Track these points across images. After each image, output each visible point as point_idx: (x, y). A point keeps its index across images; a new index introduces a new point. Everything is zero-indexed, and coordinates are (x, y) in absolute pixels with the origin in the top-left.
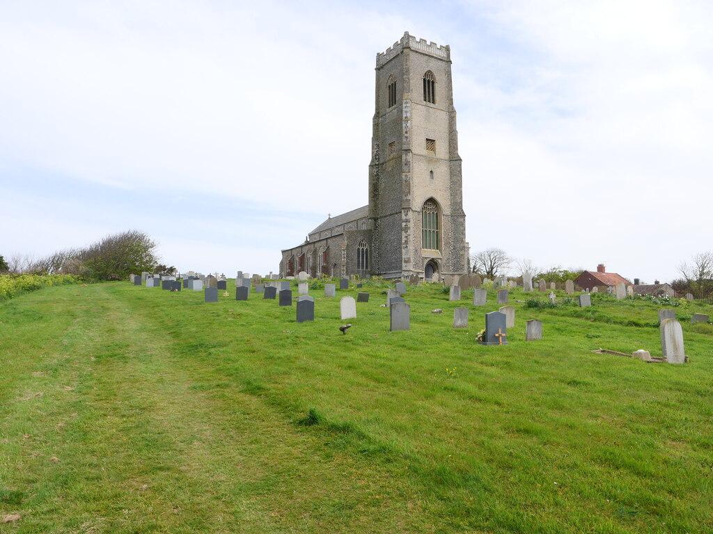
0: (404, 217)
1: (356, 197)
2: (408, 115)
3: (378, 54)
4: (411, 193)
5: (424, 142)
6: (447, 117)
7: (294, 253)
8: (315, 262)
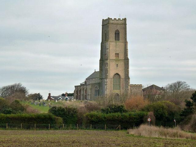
0: (106, 81)
1: (98, 69)
2: (108, 47)
3: (103, 19)
4: (108, 72)
5: (114, 55)
6: (124, 45)
7: (79, 87)
8: (83, 93)
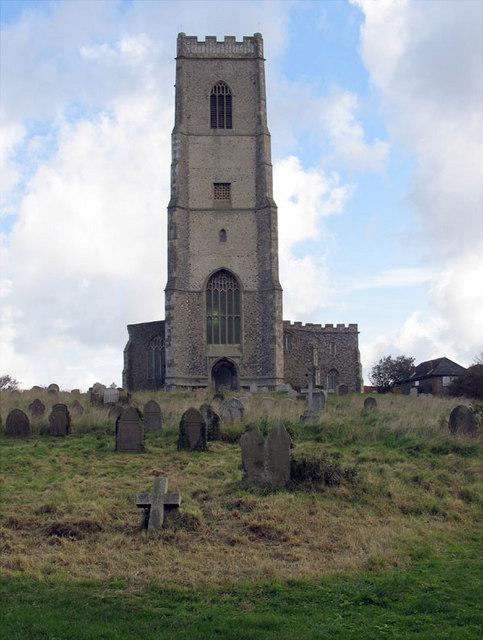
5: (211, 189)
